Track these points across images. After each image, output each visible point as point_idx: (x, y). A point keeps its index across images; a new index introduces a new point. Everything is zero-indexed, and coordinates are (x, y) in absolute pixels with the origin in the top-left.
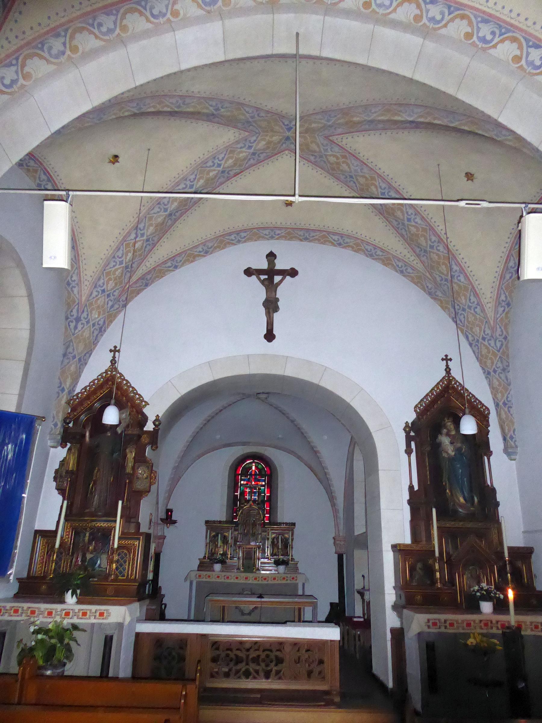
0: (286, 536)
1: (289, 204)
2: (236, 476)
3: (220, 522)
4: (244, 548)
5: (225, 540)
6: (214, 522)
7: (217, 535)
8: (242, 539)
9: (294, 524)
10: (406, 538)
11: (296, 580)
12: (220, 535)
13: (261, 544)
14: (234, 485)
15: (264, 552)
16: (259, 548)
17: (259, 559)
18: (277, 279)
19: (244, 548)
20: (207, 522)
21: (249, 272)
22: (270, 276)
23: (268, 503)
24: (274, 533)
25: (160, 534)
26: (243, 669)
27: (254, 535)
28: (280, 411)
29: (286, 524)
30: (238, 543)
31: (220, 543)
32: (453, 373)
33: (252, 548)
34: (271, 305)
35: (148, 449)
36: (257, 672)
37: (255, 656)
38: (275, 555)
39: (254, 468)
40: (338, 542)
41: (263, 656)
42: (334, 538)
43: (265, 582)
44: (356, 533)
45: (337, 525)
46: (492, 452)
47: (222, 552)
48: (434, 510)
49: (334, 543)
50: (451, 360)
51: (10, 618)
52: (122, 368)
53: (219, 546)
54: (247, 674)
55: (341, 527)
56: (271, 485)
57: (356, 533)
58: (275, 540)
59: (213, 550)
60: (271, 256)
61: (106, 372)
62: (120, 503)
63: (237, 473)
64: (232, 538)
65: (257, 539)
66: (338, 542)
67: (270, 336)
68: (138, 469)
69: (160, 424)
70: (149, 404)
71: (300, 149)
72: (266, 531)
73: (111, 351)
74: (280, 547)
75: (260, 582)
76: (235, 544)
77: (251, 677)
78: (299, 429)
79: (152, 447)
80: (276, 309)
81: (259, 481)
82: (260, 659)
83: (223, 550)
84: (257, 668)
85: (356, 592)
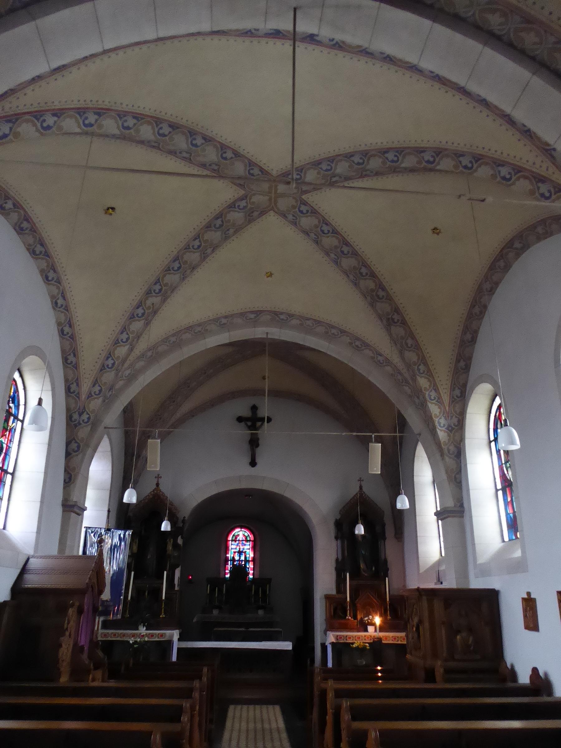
1: (264, 378)
10: (333, 592)
18: (259, 424)
21: (240, 419)
22: (253, 421)
32: (364, 489)
34: (254, 443)
46: (435, 515)
48: (348, 574)
50: (363, 480)
51: (111, 639)
52: (162, 488)
60: (254, 408)
61: (154, 491)
62: (165, 573)
67: (253, 463)
73: (156, 477)
80: (258, 445)
81: (245, 545)
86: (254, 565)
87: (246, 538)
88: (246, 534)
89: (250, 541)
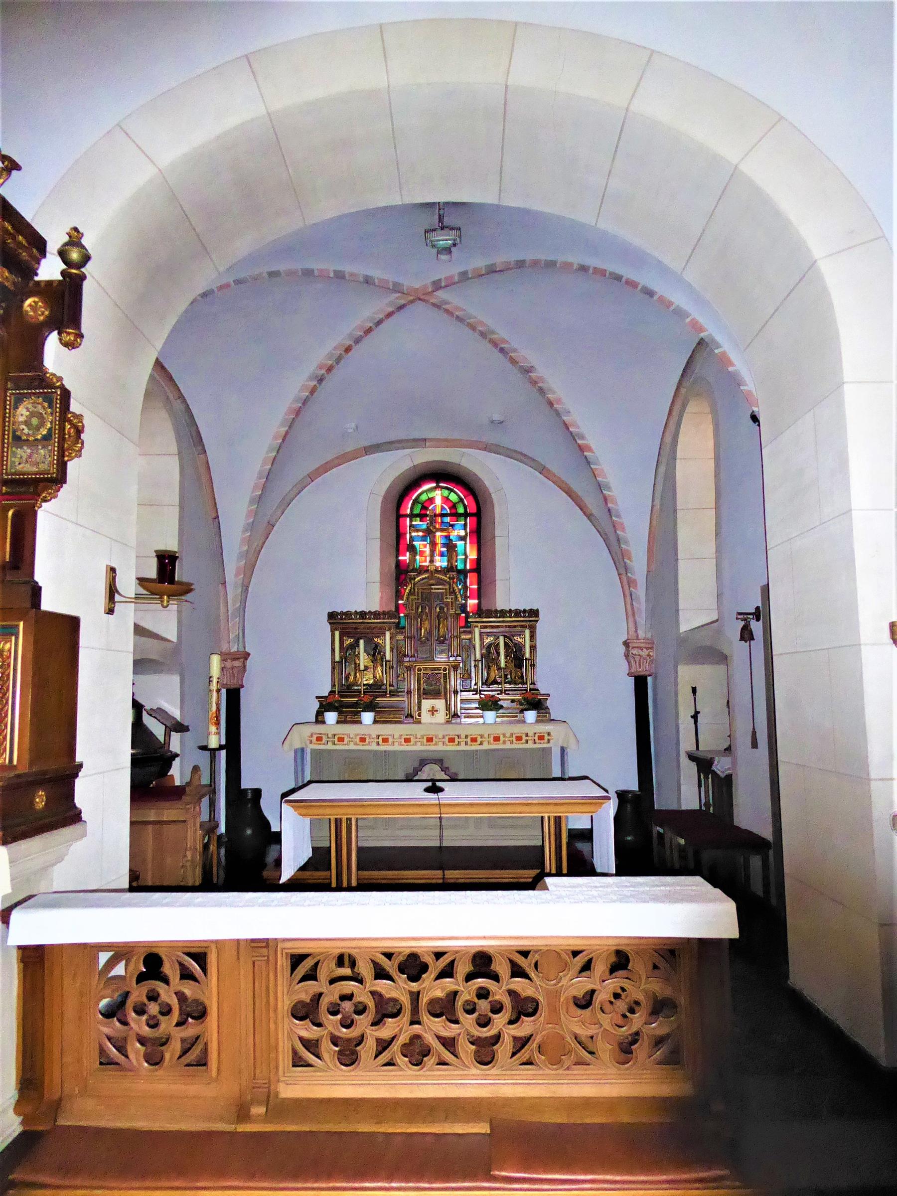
0: (518, 639)
2: (399, 516)
3: (363, 614)
4: (419, 670)
5: (376, 653)
6: (348, 614)
7: (357, 644)
8: (416, 650)
9: (535, 613)
11: (549, 741)
12: (362, 642)
13: (459, 658)
14: (398, 541)
15: (467, 676)
16: (456, 668)
17: (456, 692)
19: (419, 670)
20: (332, 616)
23: (475, 575)
24: (488, 634)
25: (234, 649)
26: (403, 1039)
27: (441, 641)
28: (495, 344)
29: (518, 613)
30: (407, 659)
31: (364, 659)
33: (438, 669)
35: (52, 342)
36: (449, 1043)
37: (439, 994)
38: (495, 682)
39: (438, 501)
40: (635, 652)
41: (467, 992)
42: (626, 644)
43: (475, 747)
44: (684, 627)
45: (631, 613)
47: (371, 682)
49: (627, 656)
53: (362, 668)
54: (417, 1053)
55: (642, 619)
56: (479, 534)
57: (684, 627)
58: (492, 650)
59: (352, 678)
63: (402, 512)
64: (392, 649)
65: (449, 650)
66: (635, 652)
68: (16, 408)
69: (86, 258)
70: (18, 167)
71: (481, 818)
72: (470, 632)
74: (503, 665)
75: (463, 747)
76: (400, 662)
77: (430, 1061)
78: (541, 391)
79: (59, 334)
82: (459, 1003)
83: (375, 677)
84: (451, 1030)
85: (684, 760)
86: (479, 583)
87: (453, 506)
88: (453, 497)
89: (465, 515)
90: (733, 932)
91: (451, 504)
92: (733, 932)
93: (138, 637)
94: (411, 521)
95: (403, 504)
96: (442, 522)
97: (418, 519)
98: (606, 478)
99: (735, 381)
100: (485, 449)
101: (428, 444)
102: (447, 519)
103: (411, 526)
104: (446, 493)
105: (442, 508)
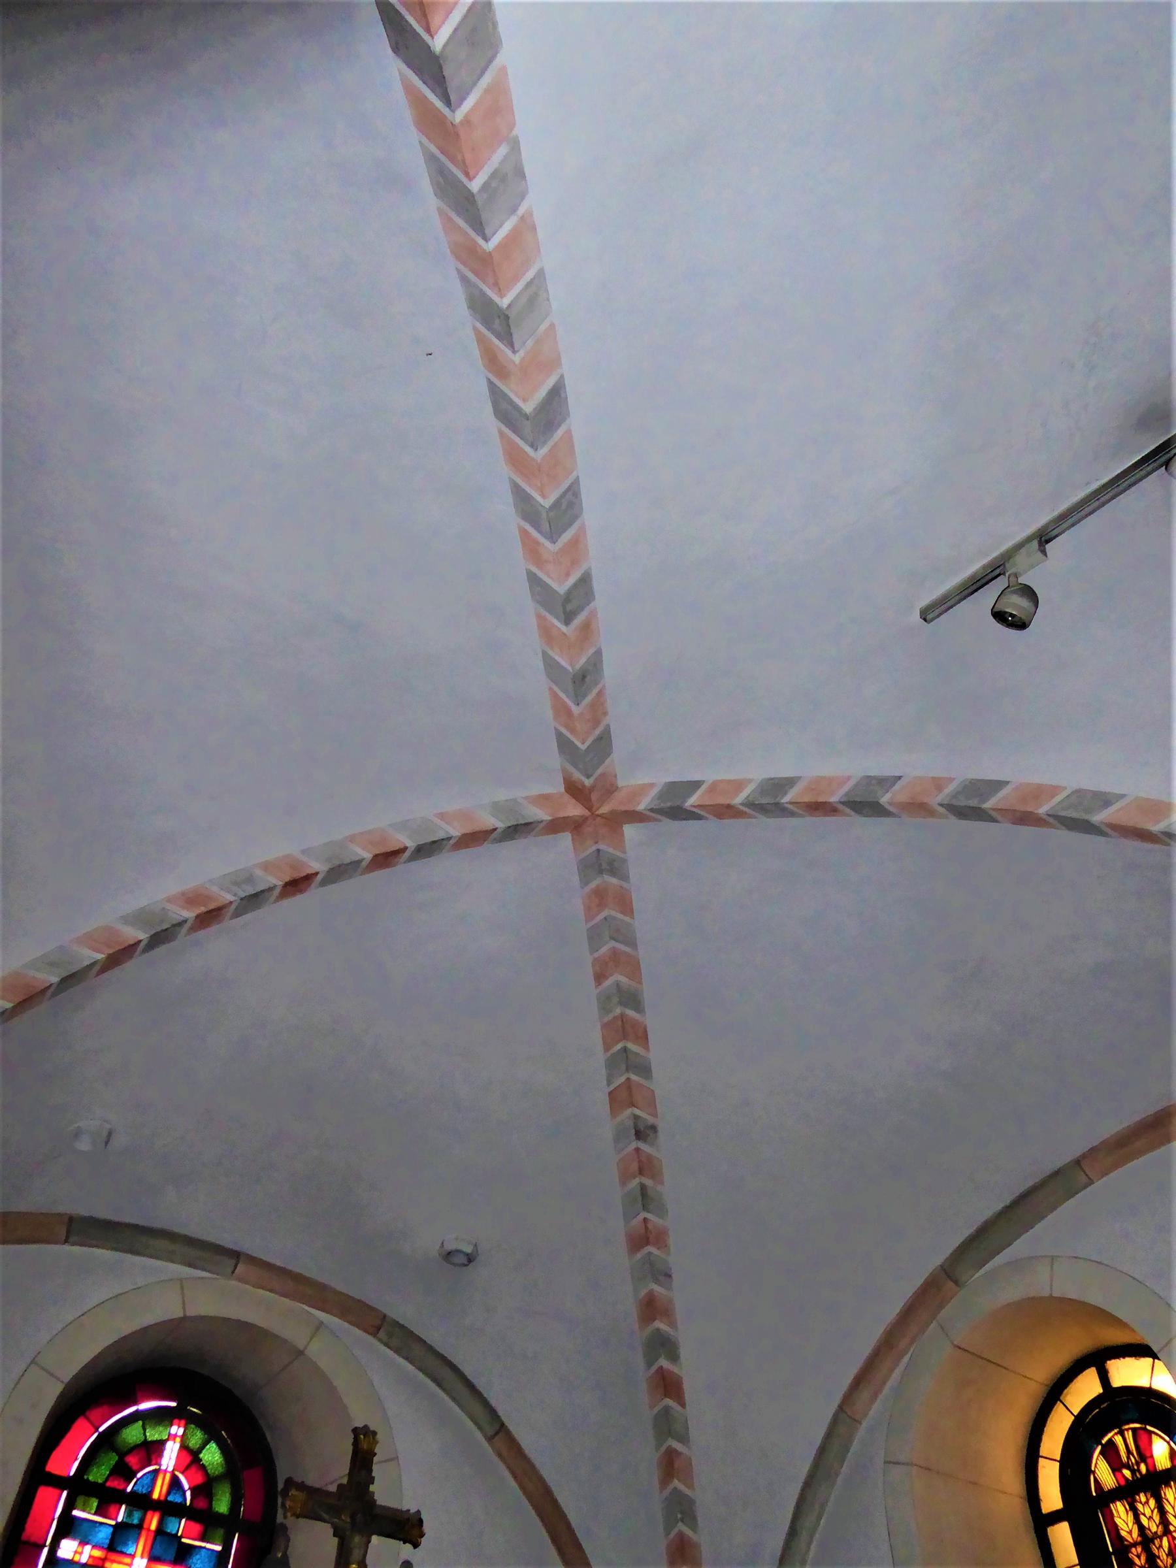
39: (170, 1456)
63: (53, 1466)
87: (204, 1490)
90: (1044, 1511)
91: (199, 1479)
92: (1044, 1511)
93: (1164, 798)
94: (70, 1505)
95: (65, 1443)
96: (160, 1531)
97: (95, 1503)
98: (691, 1487)
99: (623, 835)
100: (374, 1331)
101: (241, 1268)
102: (179, 1526)
103: (66, 1516)
104: (196, 1438)
105: (175, 1484)
